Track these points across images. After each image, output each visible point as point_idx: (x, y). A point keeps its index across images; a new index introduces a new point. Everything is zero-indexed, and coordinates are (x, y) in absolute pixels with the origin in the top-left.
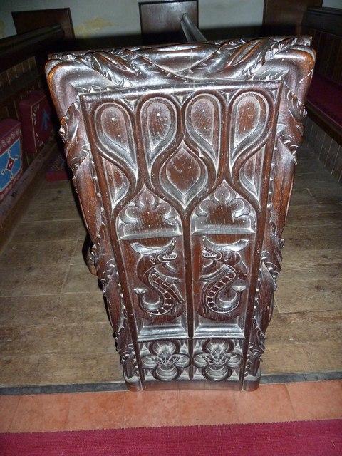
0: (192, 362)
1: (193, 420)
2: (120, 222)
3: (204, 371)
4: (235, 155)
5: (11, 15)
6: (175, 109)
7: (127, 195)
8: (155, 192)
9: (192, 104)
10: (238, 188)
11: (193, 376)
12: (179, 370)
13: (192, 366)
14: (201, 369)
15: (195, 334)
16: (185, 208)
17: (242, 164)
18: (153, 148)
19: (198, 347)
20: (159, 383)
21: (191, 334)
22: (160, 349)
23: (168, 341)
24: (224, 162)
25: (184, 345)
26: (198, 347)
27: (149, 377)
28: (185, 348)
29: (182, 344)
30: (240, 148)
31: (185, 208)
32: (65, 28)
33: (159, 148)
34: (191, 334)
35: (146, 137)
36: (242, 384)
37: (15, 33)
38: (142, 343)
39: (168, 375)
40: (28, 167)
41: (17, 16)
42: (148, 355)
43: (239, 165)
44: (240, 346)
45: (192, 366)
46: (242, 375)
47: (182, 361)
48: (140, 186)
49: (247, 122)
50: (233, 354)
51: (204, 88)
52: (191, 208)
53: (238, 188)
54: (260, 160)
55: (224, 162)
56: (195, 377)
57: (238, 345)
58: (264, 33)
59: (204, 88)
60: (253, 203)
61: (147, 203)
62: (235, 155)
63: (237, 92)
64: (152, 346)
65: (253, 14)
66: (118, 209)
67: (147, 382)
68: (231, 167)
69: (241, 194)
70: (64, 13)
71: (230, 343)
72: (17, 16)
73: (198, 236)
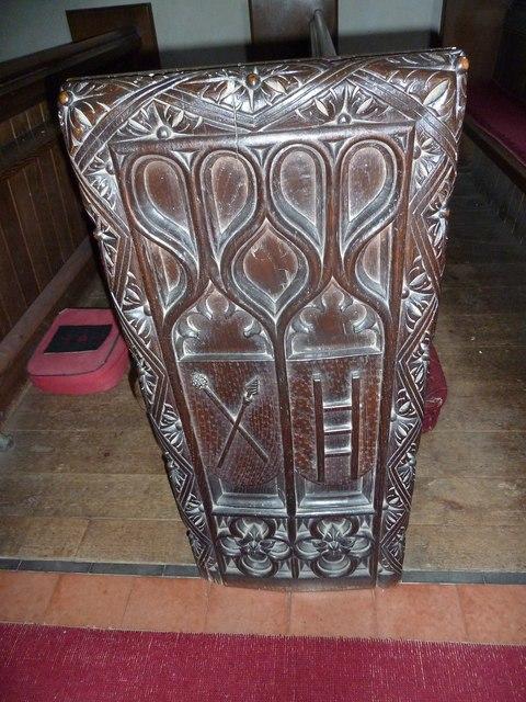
0: (293, 552)
1: (299, 628)
2: (291, 330)
3: (313, 564)
4: (350, 235)
5: (65, 19)
6: (324, 167)
7: (183, 299)
8: (229, 296)
9: (229, 155)
10: (353, 290)
11: (298, 573)
12: (275, 564)
13: (294, 558)
14: (310, 562)
15: (298, 510)
16: (275, 320)
17: (360, 249)
18: (222, 229)
19: (303, 532)
20: (245, 579)
21: (291, 508)
22: (326, 529)
23: (260, 518)
24: (332, 247)
25: (365, 524)
26: (303, 532)
27: (231, 568)
28: (282, 532)
29: (279, 524)
30: (360, 221)
31: (275, 320)
32: (141, 34)
33: (229, 231)
34: (291, 508)
35: (211, 210)
36: (373, 579)
37: (69, 40)
38: (221, 515)
39: (258, 568)
40: (61, 263)
41: (76, 18)
42: (308, 539)
43: (355, 254)
44: (369, 524)
45: (294, 558)
46: (373, 569)
47: (278, 550)
48: (203, 287)
49: (366, 181)
50: (360, 537)
51: (374, 132)
52: (285, 320)
53: (353, 290)
54: (387, 247)
55: (332, 247)
56: (302, 574)
57: (365, 524)
58: (435, 40)
59: (374, 132)
60: (372, 303)
61: (334, 299)
62: (350, 235)
63: (347, 142)
64: (235, 521)
65: (236, 30)
66: (173, 316)
67: (229, 574)
68: (343, 256)
69: (360, 298)
70: (144, 12)
71: (354, 522)
72: (76, 18)
73: (303, 369)
